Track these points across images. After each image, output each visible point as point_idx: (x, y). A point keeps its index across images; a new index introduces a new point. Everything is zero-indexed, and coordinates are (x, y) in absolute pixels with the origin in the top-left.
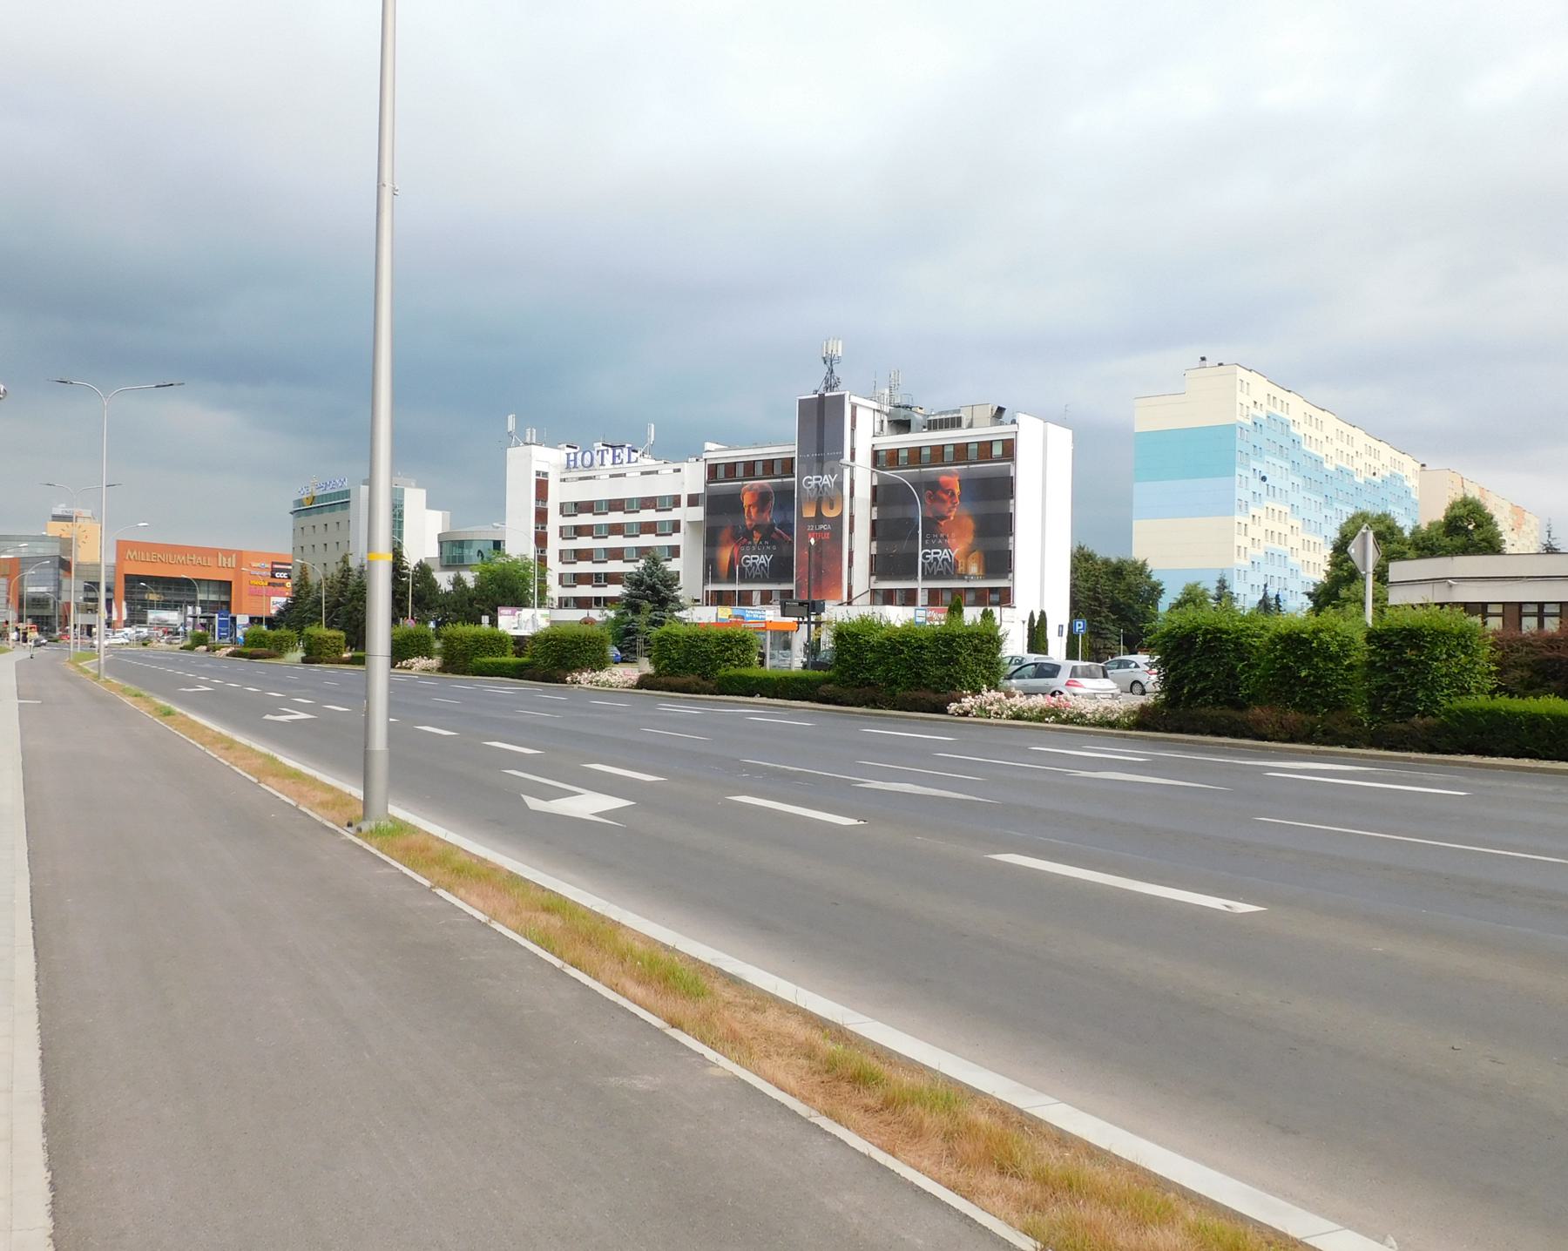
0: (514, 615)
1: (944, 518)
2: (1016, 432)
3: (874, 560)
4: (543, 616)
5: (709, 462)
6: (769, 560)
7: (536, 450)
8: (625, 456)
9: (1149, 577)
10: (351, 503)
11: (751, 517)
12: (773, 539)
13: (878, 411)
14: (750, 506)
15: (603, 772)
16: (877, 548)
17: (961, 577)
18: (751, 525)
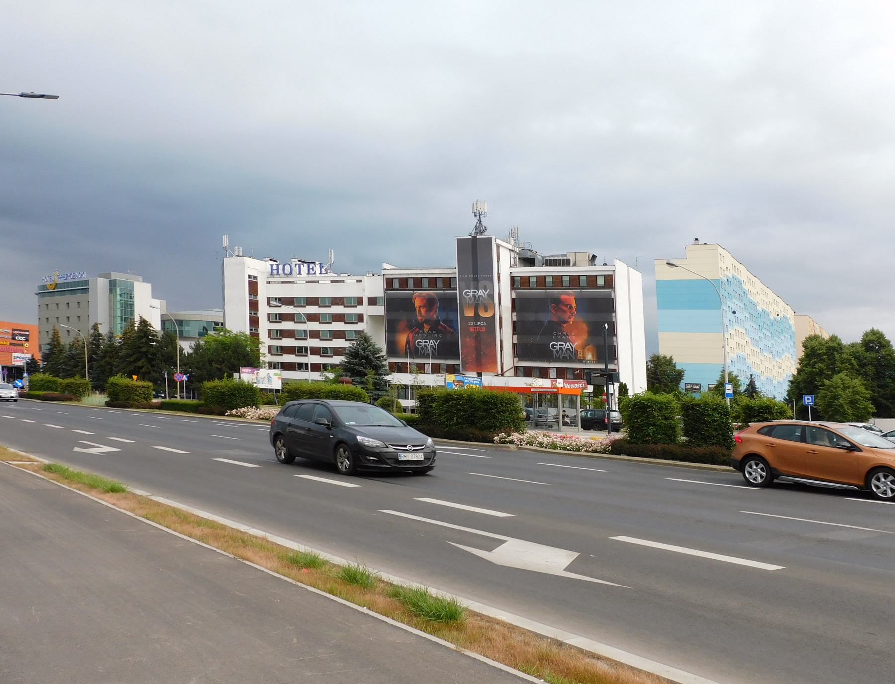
0: (253, 373)
1: (566, 322)
2: (614, 271)
3: (515, 346)
4: (275, 374)
5: (386, 276)
6: (436, 344)
7: (247, 260)
8: (318, 269)
9: (675, 366)
10: (89, 289)
11: (421, 314)
12: (438, 329)
13: (513, 251)
14: (420, 307)
15: (322, 482)
16: (518, 339)
17: (580, 361)
18: (421, 320)
